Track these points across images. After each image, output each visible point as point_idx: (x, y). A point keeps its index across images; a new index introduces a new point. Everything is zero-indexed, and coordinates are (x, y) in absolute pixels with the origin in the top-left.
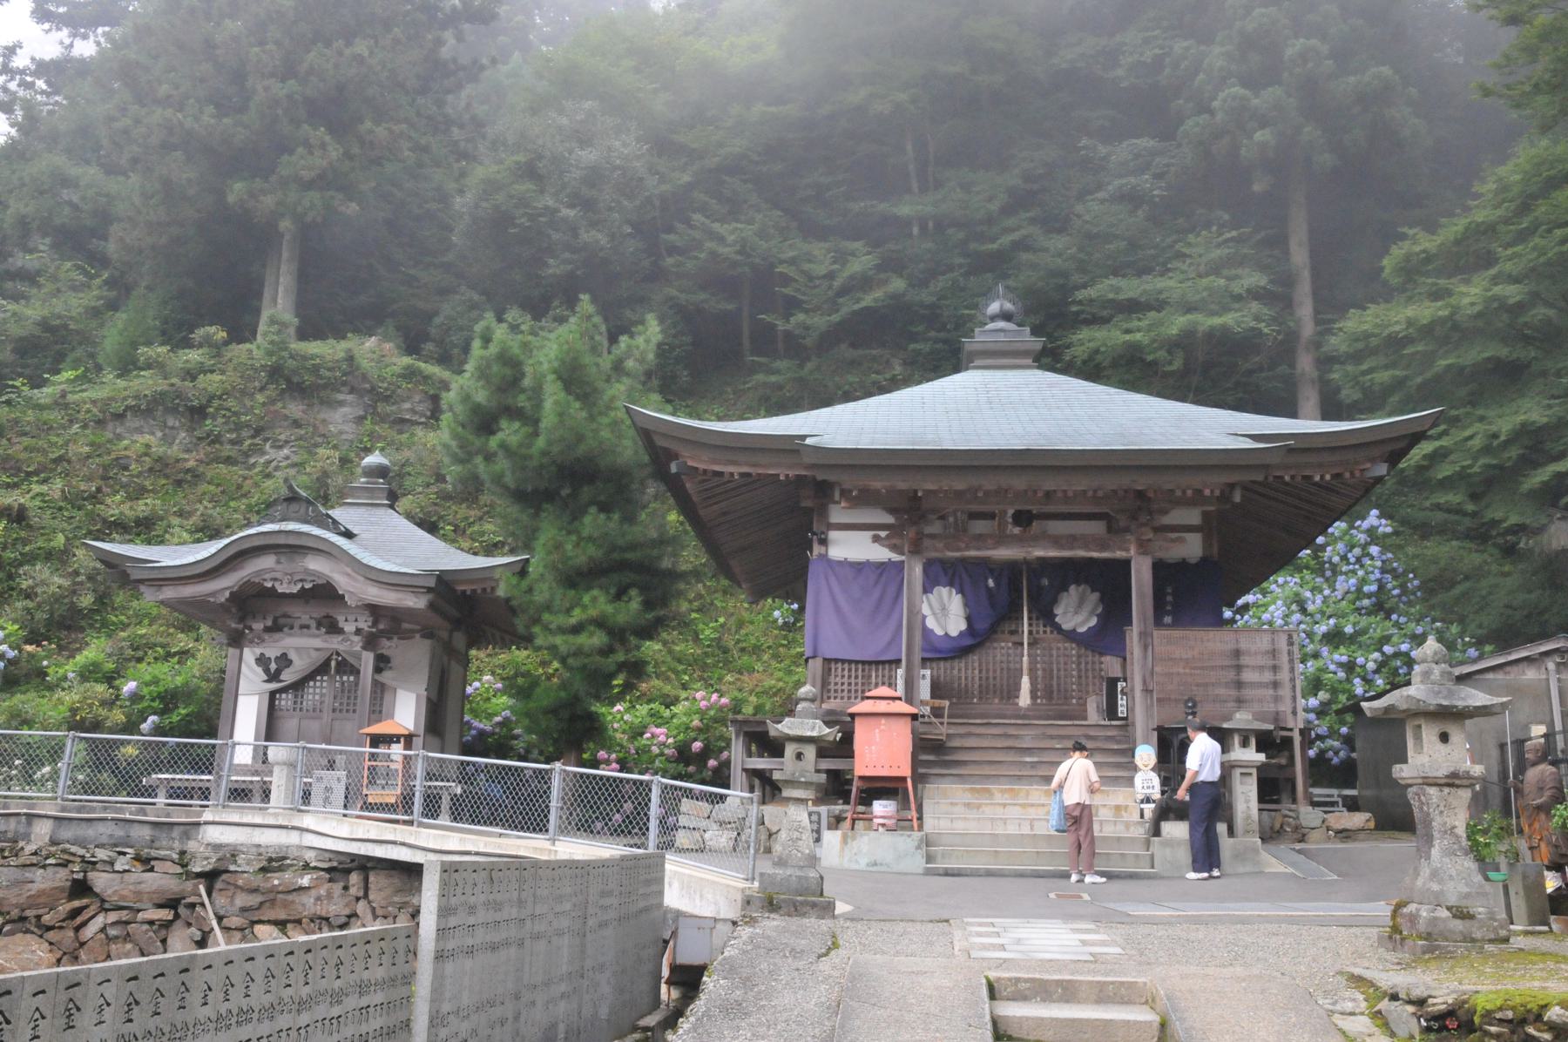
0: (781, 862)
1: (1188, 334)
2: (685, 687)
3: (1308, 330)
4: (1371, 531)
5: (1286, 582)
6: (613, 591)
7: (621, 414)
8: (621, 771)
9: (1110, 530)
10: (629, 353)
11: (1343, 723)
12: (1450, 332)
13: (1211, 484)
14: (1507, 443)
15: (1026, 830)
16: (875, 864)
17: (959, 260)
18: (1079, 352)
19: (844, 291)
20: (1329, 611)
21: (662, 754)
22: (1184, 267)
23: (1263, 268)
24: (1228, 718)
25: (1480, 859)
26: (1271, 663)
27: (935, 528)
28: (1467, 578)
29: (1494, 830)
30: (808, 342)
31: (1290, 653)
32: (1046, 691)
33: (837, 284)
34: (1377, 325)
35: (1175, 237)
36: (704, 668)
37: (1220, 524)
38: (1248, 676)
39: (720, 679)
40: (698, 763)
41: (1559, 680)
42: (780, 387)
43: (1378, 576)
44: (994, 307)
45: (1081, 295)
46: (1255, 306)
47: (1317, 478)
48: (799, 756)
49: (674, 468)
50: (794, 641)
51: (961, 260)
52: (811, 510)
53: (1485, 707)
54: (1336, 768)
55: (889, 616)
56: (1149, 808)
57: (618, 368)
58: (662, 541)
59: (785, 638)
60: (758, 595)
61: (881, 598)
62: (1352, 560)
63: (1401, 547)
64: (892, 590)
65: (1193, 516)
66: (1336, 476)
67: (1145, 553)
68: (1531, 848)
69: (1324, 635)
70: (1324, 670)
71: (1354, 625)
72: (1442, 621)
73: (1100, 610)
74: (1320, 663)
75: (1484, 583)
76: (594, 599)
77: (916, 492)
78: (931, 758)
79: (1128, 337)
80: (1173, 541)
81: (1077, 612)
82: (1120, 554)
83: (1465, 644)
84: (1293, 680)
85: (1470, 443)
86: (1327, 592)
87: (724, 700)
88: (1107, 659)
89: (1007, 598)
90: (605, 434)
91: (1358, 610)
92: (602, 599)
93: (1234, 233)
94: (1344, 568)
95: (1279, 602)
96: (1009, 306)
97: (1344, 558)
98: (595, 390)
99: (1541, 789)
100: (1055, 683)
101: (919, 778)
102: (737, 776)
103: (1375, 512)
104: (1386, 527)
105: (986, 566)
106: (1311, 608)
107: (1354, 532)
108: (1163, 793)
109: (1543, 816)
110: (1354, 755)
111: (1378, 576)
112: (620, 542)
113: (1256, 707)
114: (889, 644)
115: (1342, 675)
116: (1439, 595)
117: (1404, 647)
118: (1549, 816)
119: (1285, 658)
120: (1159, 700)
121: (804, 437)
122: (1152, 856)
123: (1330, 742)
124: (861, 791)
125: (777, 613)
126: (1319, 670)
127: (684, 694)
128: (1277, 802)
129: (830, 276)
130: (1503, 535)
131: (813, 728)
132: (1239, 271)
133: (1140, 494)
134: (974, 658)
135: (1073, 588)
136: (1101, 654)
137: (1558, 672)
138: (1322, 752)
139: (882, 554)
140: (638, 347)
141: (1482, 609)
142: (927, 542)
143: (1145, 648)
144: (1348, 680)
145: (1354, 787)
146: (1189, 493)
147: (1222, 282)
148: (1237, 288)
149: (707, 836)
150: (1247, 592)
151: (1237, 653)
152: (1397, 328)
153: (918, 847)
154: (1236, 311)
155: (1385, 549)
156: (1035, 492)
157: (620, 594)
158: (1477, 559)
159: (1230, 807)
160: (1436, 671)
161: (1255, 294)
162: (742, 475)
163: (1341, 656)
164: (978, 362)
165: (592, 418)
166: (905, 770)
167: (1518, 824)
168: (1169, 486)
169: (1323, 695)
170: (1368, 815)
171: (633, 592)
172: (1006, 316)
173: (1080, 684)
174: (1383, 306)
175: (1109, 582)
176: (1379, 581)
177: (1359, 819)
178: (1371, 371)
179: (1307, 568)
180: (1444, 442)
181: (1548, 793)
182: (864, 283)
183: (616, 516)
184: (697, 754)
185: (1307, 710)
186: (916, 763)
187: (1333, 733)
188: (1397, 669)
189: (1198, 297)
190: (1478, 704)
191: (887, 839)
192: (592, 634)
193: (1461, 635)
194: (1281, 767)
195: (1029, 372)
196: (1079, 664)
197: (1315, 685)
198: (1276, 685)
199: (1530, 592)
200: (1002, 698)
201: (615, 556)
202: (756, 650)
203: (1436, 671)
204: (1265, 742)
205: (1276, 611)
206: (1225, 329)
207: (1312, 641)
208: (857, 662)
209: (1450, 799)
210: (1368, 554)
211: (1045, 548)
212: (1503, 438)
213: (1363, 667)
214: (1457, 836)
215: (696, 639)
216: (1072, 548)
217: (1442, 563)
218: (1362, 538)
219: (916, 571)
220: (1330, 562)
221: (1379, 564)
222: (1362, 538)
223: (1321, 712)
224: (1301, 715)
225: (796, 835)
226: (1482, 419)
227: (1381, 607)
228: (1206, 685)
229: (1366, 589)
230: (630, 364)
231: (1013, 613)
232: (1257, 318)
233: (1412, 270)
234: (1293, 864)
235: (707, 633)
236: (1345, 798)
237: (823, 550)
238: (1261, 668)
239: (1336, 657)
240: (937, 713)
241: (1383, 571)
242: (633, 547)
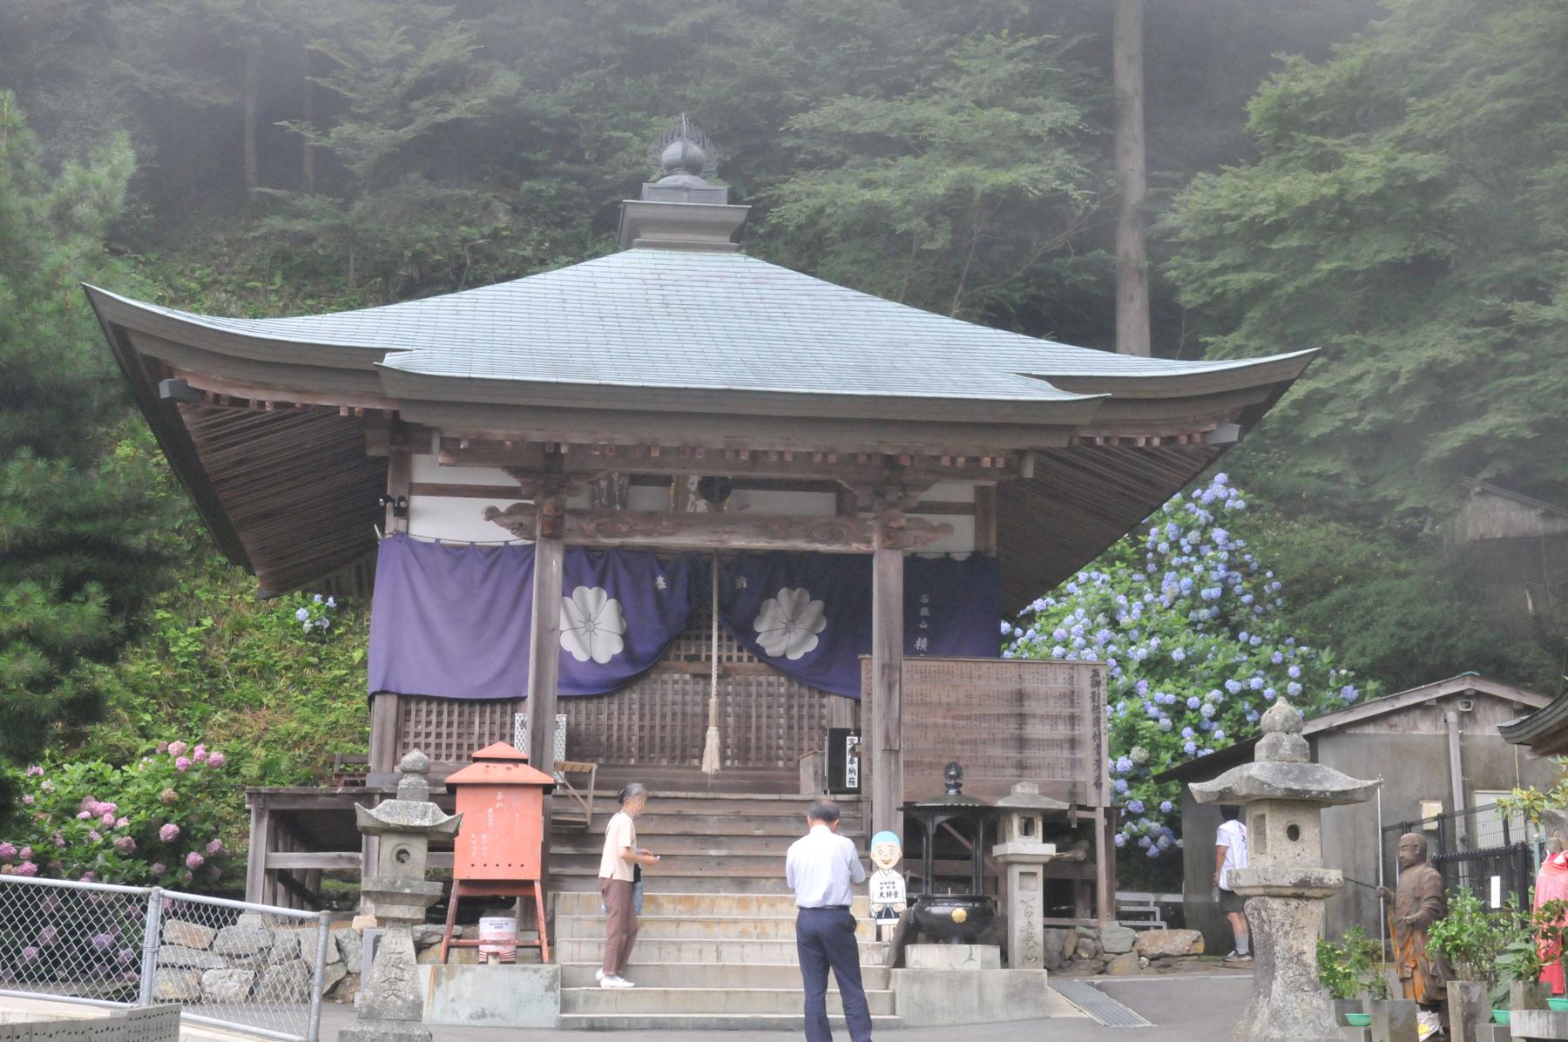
0: (371, 1015)
1: (961, 196)
2: (144, 733)
3: (1136, 192)
4: (1215, 506)
5: (1090, 579)
6: (55, 584)
7: (75, 298)
8: (37, 875)
9: (840, 510)
10: (81, 194)
11: (1165, 795)
12: (1341, 218)
13: (993, 451)
14: (1408, 390)
15: (710, 960)
16: (483, 1015)
17: (607, 49)
18: (791, 213)
19: (422, 88)
20: (1150, 626)
21: (108, 844)
22: (957, 88)
23: (1074, 95)
24: (1005, 792)
25: (1338, 996)
26: (1067, 711)
27: (578, 501)
28: (1348, 579)
29: (1356, 955)
30: (358, 168)
31: (1094, 696)
32: (738, 749)
33: (409, 76)
34: (1235, 205)
35: (943, 37)
36: (178, 699)
37: (1000, 503)
38: (1035, 730)
39: (203, 719)
40: (182, 857)
41: (1462, 737)
42: (308, 239)
43: (1223, 573)
44: (673, 151)
45: (801, 121)
46: (1060, 156)
47: (1141, 443)
48: (402, 855)
49: (165, 391)
50: (329, 658)
51: (611, 50)
52: (382, 461)
53: (1344, 792)
54: (1153, 860)
55: (504, 629)
56: (890, 926)
57: (63, 218)
58: (139, 507)
59: (315, 652)
60: (280, 585)
61: (492, 602)
62: (1187, 549)
63: (1257, 530)
64: (509, 590)
65: (963, 492)
66: (1168, 441)
67: (892, 547)
68: (1403, 980)
69: (1142, 663)
70: (1141, 715)
71: (1186, 647)
72: (1311, 643)
73: (821, 628)
74: (1135, 705)
75: (1371, 588)
76: (24, 600)
77: (557, 446)
78: (568, 850)
79: (868, 195)
80: (934, 529)
81: (788, 631)
82: (857, 547)
83: (1339, 679)
84: (1097, 736)
85: (1359, 386)
86: (1148, 597)
87: (216, 755)
88: (832, 701)
89: (685, 609)
90: (46, 329)
91: (1193, 624)
92: (39, 599)
93: (1034, 41)
94: (1175, 561)
95: (1080, 611)
96: (695, 150)
97: (1175, 545)
98: (27, 254)
99: (1418, 899)
100: (753, 736)
101: (551, 882)
102: (257, 880)
103: (1221, 477)
104: (1236, 501)
105: (656, 559)
106: (1125, 620)
107: (1190, 506)
108: (910, 902)
109: (1418, 937)
110: (1179, 842)
111: (1223, 573)
112: (69, 505)
113: (1044, 776)
114: (504, 671)
115: (1166, 722)
116: (1311, 603)
117: (1255, 683)
118: (1426, 937)
119: (1087, 705)
120: (908, 765)
121: (381, 353)
122: (893, 996)
123: (1145, 824)
124: (462, 901)
125: (301, 613)
126: (1135, 715)
127: (145, 746)
128: (1070, 914)
129: (399, 63)
130: (1402, 516)
131: (424, 815)
132: (1039, 100)
133: (890, 462)
134: (632, 696)
135: (783, 591)
136: (822, 694)
137: (1461, 725)
138: (1134, 838)
139: (498, 535)
140: (98, 186)
141: (1366, 626)
142: (569, 522)
143: (890, 686)
144: (1175, 730)
145: (1178, 891)
146: (961, 461)
147: (1014, 116)
148: (1034, 126)
149: (205, 977)
150: (1040, 594)
151: (1021, 696)
152: (1263, 209)
153: (550, 988)
154: (1032, 162)
155: (1234, 532)
156: (737, 452)
157: (69, 590)
158: (1363, 549)
159: (1004, 921)
160: (1287, 742)
161: (1060, 136)
162: (277, 405)
163: (1166, 694)
164: (645, 237)
165: (22, 302)
166: (532, 871)
167: (1388, 946)
168: (935, 452)
169: (1138, 753)
170: (1195, 934)
171: (93, 588)
172: (693, 167)
173: (790, 738)
174: (1244, 171)
175: (841, 590)
176: (1224, 581)
177: (1183, 940)
178: (1223, 270)
179: (1122, 558)
180: (1320, 383)
181: (1426, 905)
182: (450, 79)
183: (63, 464)
184: (168, 844)
185: (1115, 775)
186: (547, 859)
187: (1150, 810)
188: (1243, 715)
189: (977, 136)
190: (1337, 788)
191: (501, 976)
192: (19, 655)
193: (1336, 664)
194: (1076, 863)
195: (724, 257)
197: (1128, 737)
198: (1073, 743)
199: (1432, 602)
200: (673, 758)
201: (61, 527)
202: (265, 672)
203: (1287, 742)
204: (1056, 827)
205: (1074, 623)
206: (1015, 192)
207: (1125, 671)
208: (451, 701)
209: (1298, 915)
210: (1210, 541)
212: (1402, 382)
213: (1196, 710)
214: (1305, 966)
215: (164, 653)
216: (786, 537)
217: (1313, 559)
218: (1202, 515)
219: (551, 563)
220: (1155, 551)
221: (1224, 555)
222: (1202, 515)
223: (1135, 778)
224: (1107, 782)
225: (395, 972)
226: (1375, 351)
227: (1226, 622)
228: (974, 742)
229: (1205, 593)
230: (82, 210)
231: (695, 627)
232: (1064, 176)
233: (1287, 120)
234: (1091, 1006)
235: (184, 643)
236: (1164, 907)
237: (402, 523)
238: (1054, 719)
239: (1159, 695)
240: (577, 781)
241: (1231, 567)
242: (90, 515)
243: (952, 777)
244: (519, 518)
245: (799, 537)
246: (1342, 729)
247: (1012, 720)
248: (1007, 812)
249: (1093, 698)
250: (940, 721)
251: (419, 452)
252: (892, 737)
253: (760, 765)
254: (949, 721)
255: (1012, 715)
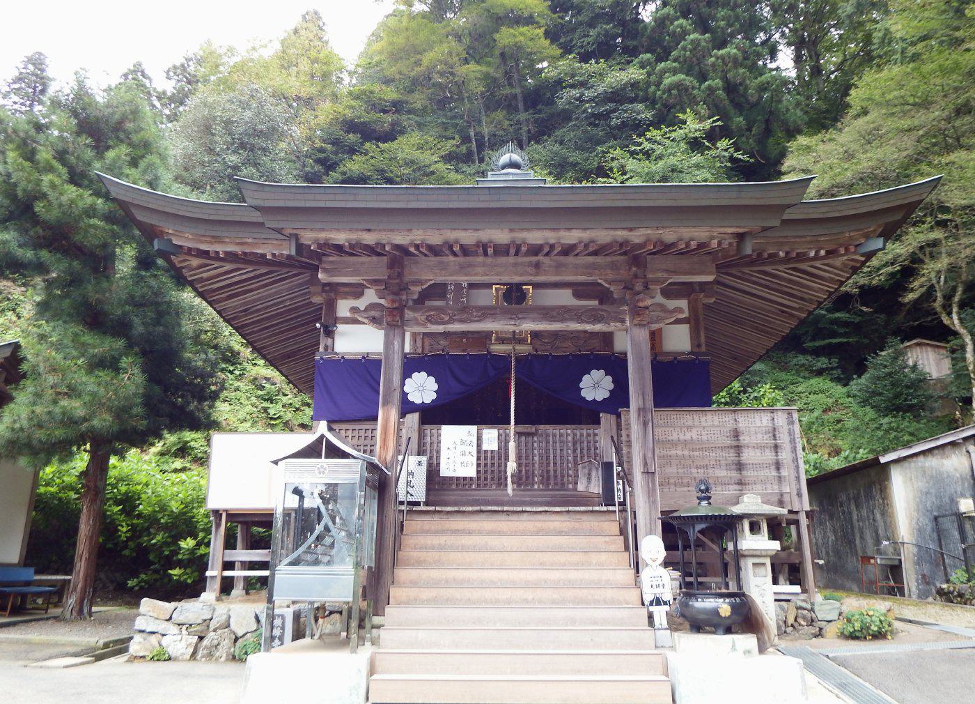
143: (645, 425)
196: (575, 450)
211: (534, 320)
243: (702, 491)
244: (373, 313)
245: (572, 320)
246: (905, 458)
247: (732, 451)
248: (740, 518)
249: (790, 435)
250: (680, 453)
251: (342, 298)
252: (649, 461)
253: (557, 487)
254: (686, 452)
255: (731, 447)
